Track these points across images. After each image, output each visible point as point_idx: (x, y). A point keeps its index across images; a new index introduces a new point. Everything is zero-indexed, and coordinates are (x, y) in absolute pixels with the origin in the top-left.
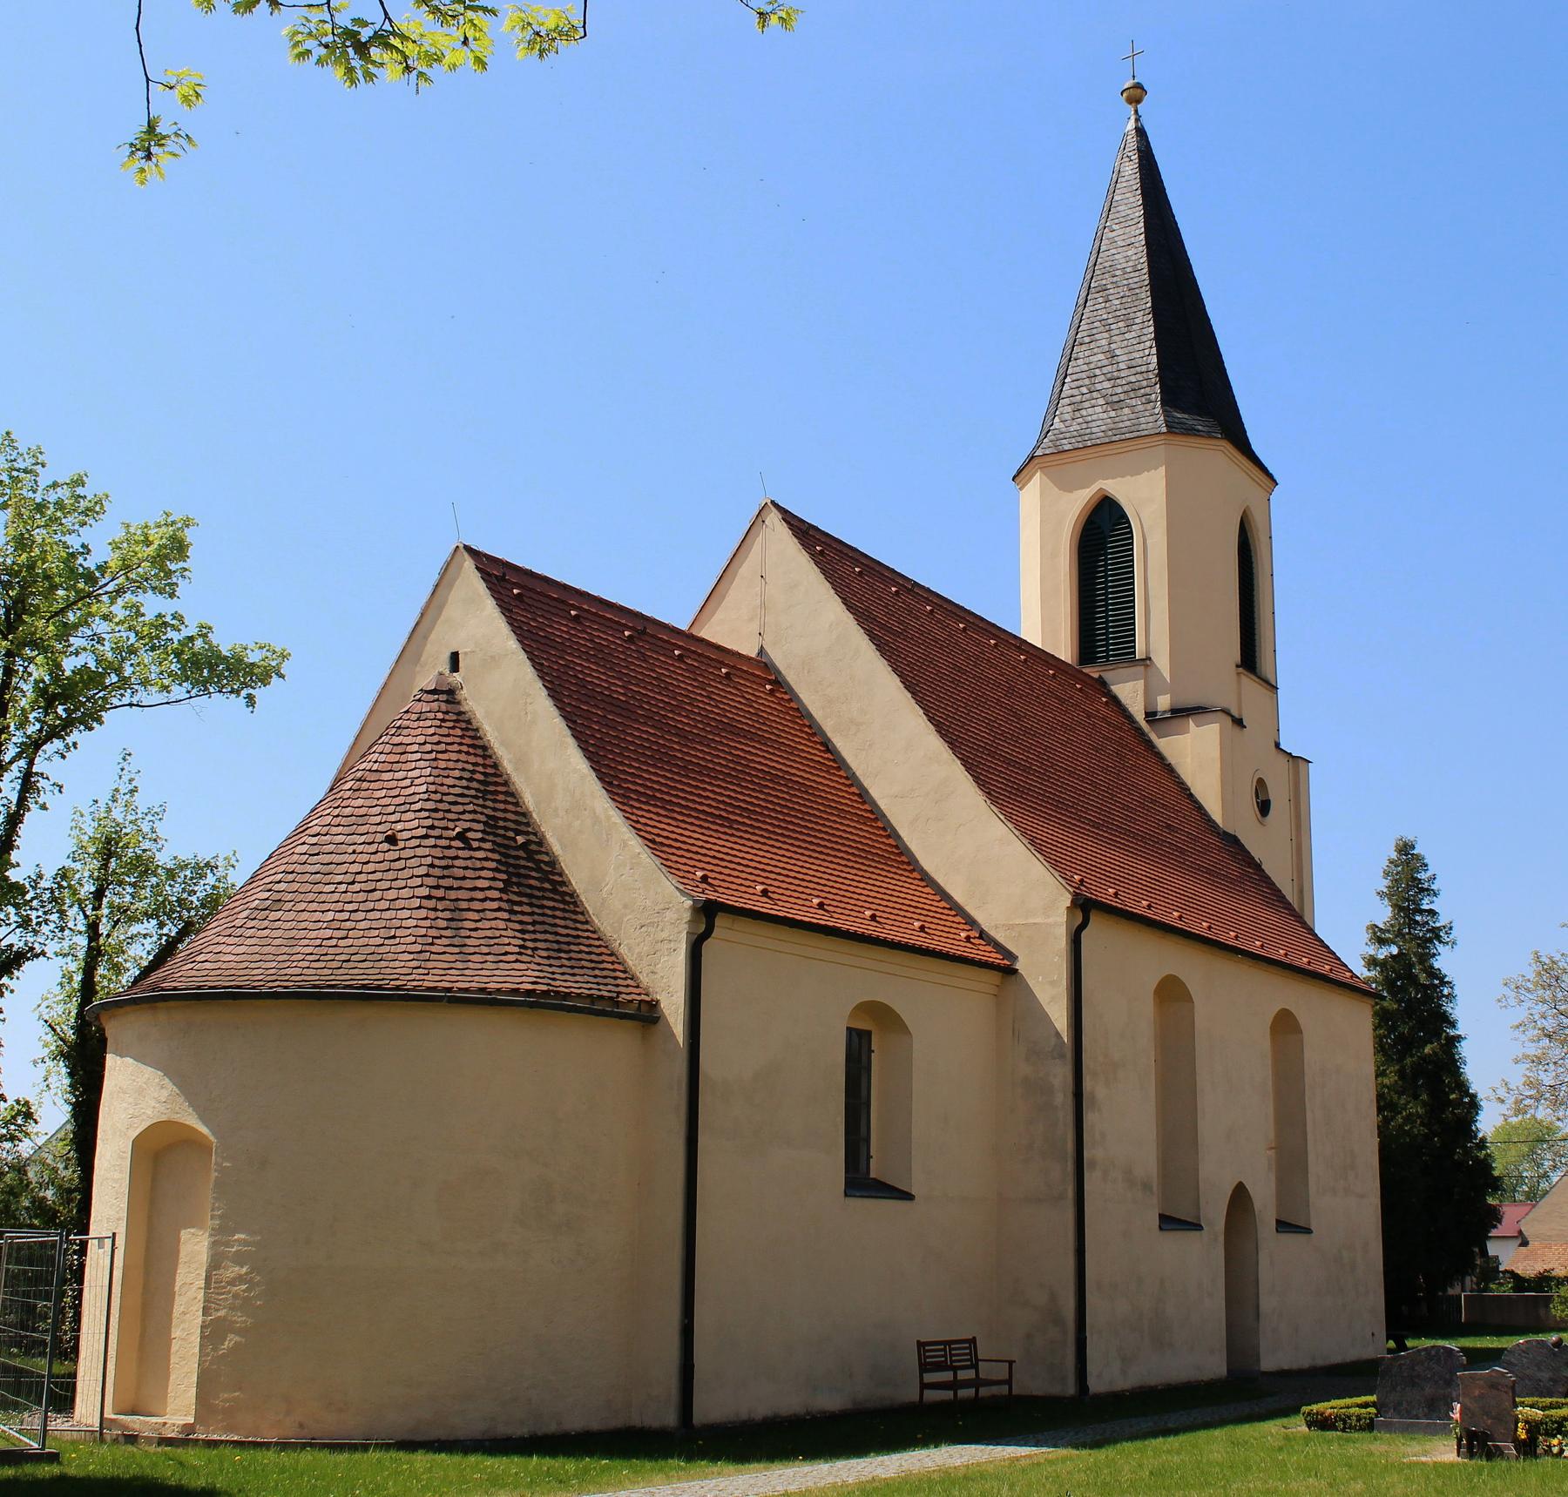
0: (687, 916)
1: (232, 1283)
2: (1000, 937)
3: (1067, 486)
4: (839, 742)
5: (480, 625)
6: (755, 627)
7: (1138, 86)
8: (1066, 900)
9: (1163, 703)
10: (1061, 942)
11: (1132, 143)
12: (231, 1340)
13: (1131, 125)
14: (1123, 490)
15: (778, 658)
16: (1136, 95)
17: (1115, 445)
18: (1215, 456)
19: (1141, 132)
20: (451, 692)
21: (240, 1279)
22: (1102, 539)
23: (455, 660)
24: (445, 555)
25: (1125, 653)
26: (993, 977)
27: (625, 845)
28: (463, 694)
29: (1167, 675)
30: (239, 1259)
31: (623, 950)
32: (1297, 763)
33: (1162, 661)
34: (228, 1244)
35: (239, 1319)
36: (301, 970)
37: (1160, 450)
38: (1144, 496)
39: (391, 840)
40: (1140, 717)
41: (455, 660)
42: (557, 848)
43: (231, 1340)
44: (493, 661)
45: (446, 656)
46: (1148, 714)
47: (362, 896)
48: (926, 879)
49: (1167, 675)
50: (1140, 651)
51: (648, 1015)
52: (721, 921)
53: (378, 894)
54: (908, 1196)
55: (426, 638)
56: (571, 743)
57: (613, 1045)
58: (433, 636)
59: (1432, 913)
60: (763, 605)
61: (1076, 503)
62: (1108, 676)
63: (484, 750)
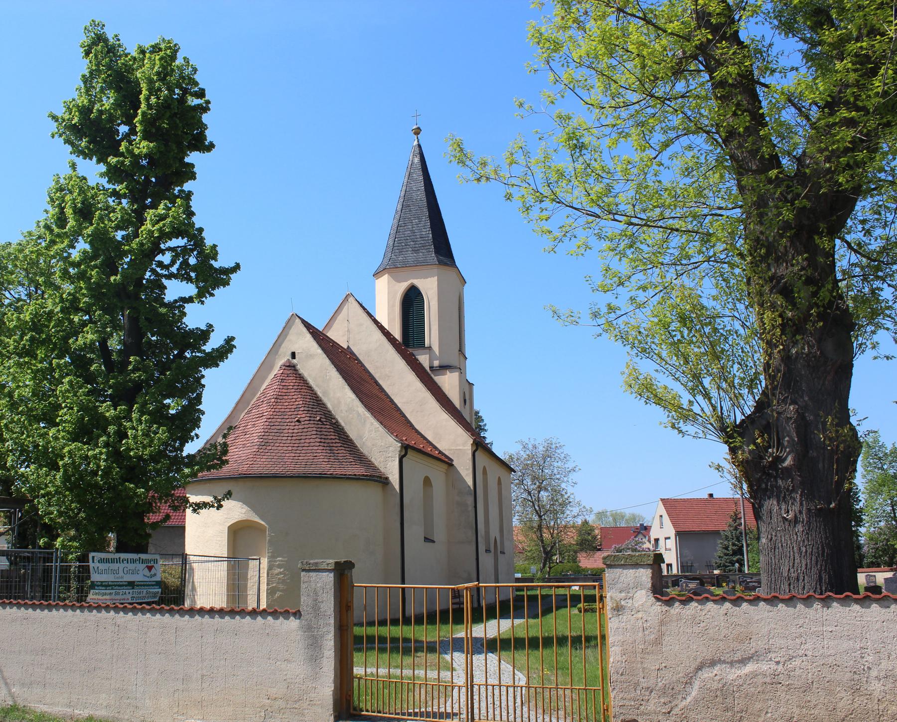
0: (399, 449)
1: (277, 574)
2: (447, 453)
3: (399, 281)
4: (381, 382)
5: (304, 343)
6: (345, 338)
7: (419, 128)
8: (471, 441)
9: (436, 363)
10: (470, 456)
11: (417, 151)
12: (278, 594)
13: (416, 143)
14: (420, 283)
15: (355, 350)
16: (417, 131)
17: (418, 265)
18: (447, 271)
19: (419, 146)
20: (294, 366)
21: (281, 573)
22: (412, 301)
23: (293, 355)
24: (288, 317)
25: (421, 344)
26: (445, 466)
27: (372, 424)
28: (298, 367)
29: (437, 353)
30: (279, 566)
31: (373, 460)
32: (471, 385)
33: (436, 348)
34: (275, 561)
35: (281, 586)
36: (300, 470)
37: (435, 270)
38: (429, 287)
39: (298, 421)
40: (428, 369)
41: (293, 355)
42: (343, 424)
43: (278, 594)
44: (310, 356)
45: (290, 353)
46: (430, 368)
47: (298, 442)
48: (417, 431)
49: (437, 353)
50: (427, 344)
51: (384, 481)
52: (410, 452)
53: (302, 441)
54: (433, 542)
55: (280, 346)
56: (347, 387)
57: (370, 494)
58: (283, 345)
59: (484, 438)
60: (348, 331)
61: (403, 287)
62: (415, 352)
63: (310, 388)
